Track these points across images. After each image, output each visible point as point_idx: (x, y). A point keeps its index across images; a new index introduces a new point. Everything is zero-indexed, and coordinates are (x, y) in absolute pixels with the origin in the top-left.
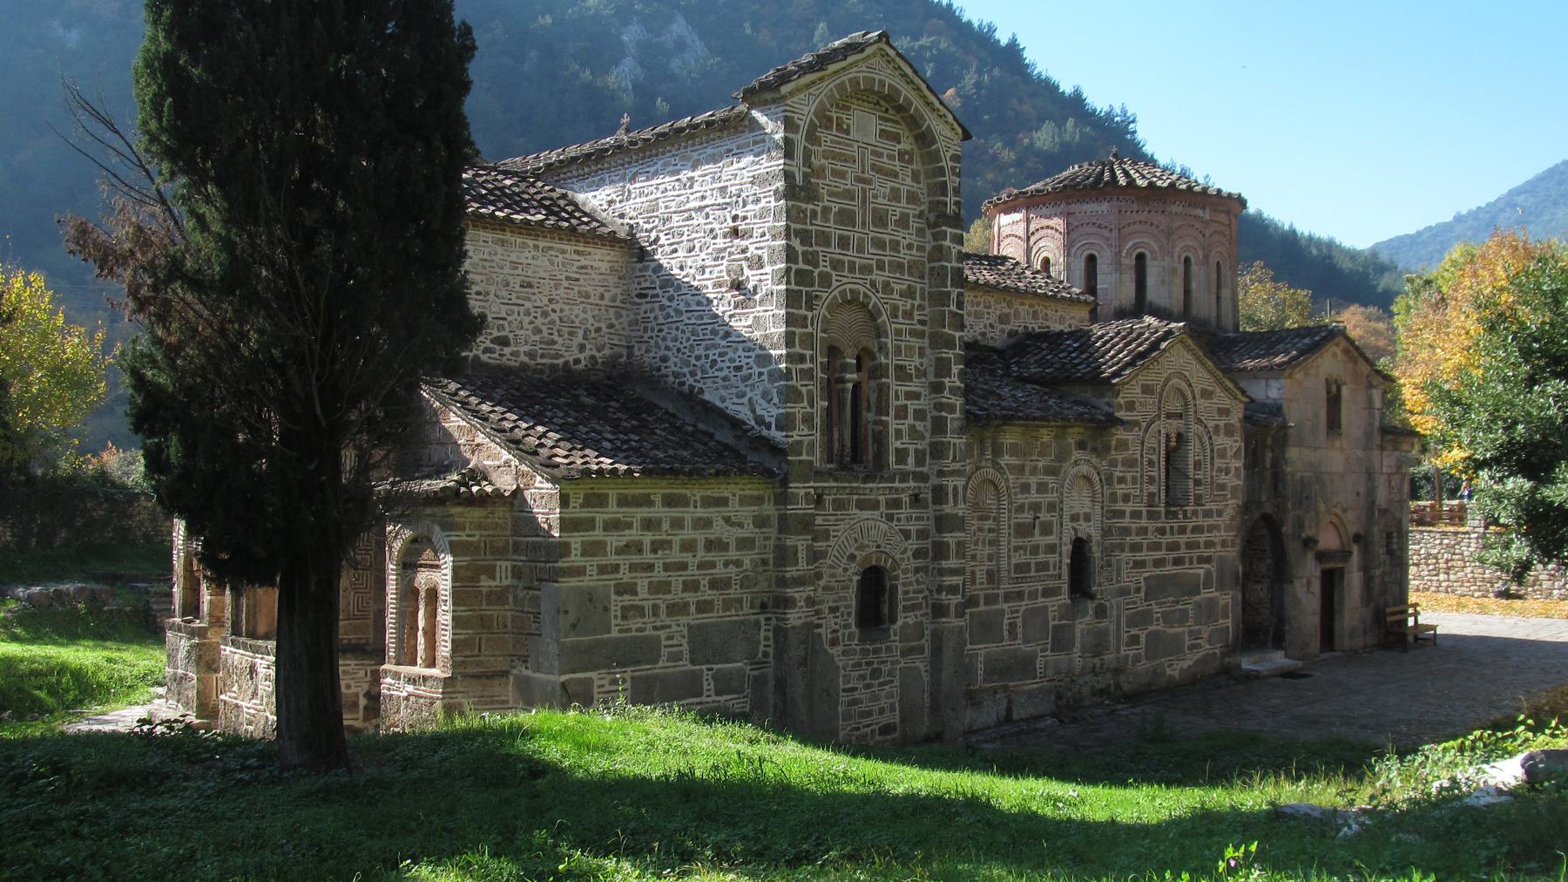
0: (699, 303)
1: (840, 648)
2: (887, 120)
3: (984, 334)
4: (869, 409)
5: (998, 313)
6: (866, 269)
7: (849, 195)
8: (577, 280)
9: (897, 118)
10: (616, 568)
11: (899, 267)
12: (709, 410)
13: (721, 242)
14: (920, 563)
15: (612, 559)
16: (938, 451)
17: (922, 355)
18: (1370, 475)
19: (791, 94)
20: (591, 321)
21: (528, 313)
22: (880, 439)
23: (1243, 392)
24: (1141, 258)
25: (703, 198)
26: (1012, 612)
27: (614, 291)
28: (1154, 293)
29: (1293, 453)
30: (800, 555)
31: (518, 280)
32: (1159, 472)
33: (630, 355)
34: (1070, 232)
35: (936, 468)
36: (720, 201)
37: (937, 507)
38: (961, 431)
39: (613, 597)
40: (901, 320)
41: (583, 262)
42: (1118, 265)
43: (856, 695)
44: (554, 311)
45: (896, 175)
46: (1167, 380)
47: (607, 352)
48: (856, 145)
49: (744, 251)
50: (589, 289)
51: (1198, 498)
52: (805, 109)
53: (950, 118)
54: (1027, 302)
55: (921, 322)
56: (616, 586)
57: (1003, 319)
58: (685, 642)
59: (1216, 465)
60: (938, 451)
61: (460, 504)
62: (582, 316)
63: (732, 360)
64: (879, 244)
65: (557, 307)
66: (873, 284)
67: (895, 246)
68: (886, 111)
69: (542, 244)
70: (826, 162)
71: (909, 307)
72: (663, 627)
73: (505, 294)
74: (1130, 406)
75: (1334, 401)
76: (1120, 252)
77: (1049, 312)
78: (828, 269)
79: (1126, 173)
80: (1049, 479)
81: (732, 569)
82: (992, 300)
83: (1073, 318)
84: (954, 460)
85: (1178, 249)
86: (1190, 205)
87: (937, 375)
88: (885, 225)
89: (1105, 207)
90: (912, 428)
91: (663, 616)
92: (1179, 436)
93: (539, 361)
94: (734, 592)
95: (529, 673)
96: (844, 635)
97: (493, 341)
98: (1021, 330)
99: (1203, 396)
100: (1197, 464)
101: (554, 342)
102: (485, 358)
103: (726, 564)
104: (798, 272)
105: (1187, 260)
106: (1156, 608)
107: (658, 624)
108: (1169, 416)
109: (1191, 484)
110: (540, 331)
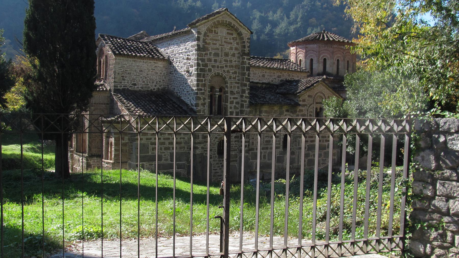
0: (181, 76)
1: (213, 159)
2: (229, 30)
3: (272, 81)
4: (223, 102)
5: (277, 75)
6: (222, 67)
7: (217, 49)
8: (154, 69)
9: (232, 29)
10: (151, 139)
12: (183, 102)
13: (185, 61)
14: (236, 139)
15: (149, 137)
19: (199, 25)
20: (158, 79)
21: (141, 78)
22: (226, 109)
23: (342, 97)
24: (325, 60)
25: (182, 50)
26: (264, 152)
27: (164, 72)
28: (328, 69)
30: (200, 137)
31: (139, 70)
33: (168, 87)
34: (306, 52)
36: (185, 51)
38: (248, 107)
39: (150, 145)
40: (232, 80)
41: (156, 65)
42: (318, 62)
43: (217, 171)
44: (148, 77)
45: (231, 43)
46: (317, 94)
47: (162, 87)
48: (220, 37)
49: (189, 63)
50: (158, 72)
52: (203, 29)
53: (247, 29)
54: (287, 72)
55: (238, 80)
56: (151, 143)
57: (279, 77)
58: (169, 156)
61: (116, 123)
62: (156, 78)
63: (187, 90)
64: (226, 61)
65: (149, 76)
66: (224, 71)
67: (231, 61)
68: (229, 28)
69: (145, 61)
70: (210, 41)
71: (235, 76)
72: (163, 153)
73: (135, 73)
74: (304, 101)
76: (319, 58)
77: (294, 75)
78: (211, 68)
79: (327, 37)
81: (182, 140)
82: (275, 72)
83: (301, 76)
86: (340, 45)
87: (242, 93)
88: (228, 56)
89: (315, 45)
90: (235, 106)
91: (163, 150)
93: (144, 89)
94: (183, 145)
95: (131, 162)
96: (213, 156)
97: (132, 84)
98: (284, 80)
101: (148, 85)
102: (130, 88)
103: (180, 138)
104: (200, 69)
105: (338, 60)
106: (311, 153)
107: (162, 152)
110: (144, 82)
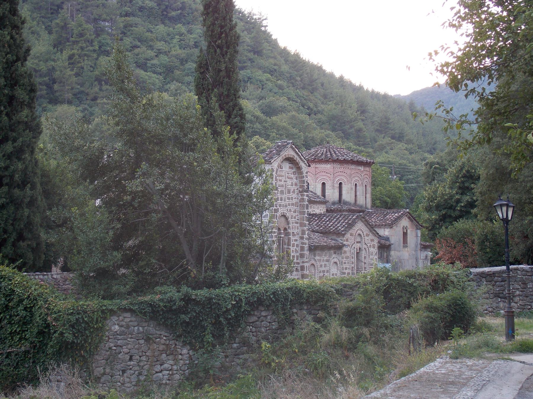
4: (285, 244)
6: (286, 206)
11: (293, 204)
16: (302, 256)
17: (298, 229)
18: (417, 259)
24: (341, 184)
29: (392, 253)
32: (354, 260)
35: (302, 261)
37: (302, 272)
51: (365, 268)
55: (298, 219)
59: (370, 258)
60: (302, 256)
75: (405, 234)
80: (327, 263)
84: (306, 258)
85: (353, 181)
88: (290, 193)
92: (360, 248)
99: (366, 236)
100: (365, 257)
105: (356, 184)
108: (357, 242)
109: (363, 263)
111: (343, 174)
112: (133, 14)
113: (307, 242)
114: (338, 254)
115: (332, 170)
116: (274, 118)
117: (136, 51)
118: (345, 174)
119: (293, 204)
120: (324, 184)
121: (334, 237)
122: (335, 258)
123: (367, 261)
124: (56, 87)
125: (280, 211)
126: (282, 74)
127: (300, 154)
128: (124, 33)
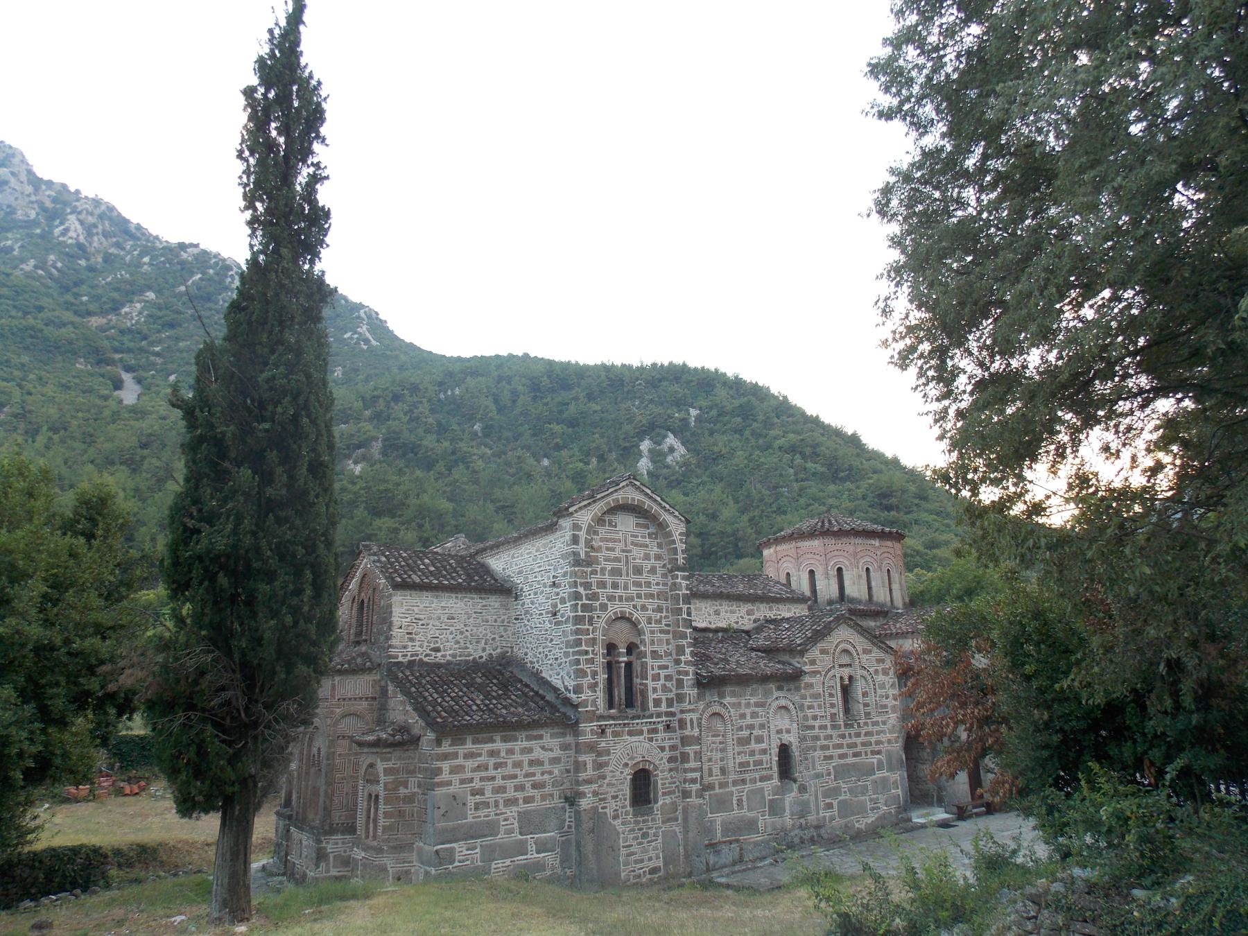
24: (840, 570)
51: (867, 715)
105: (868, 569)
109: (861, 707)
111: (841, 553)
112: (807, 479)
113: (691, 669)
114: (789, 690)
115: (822, 549)
116: (935, 551)
117: (810, 508)
118: (845, 554)
119: (651, 596)
120: (812, 572)
121: (786, 658)
122: (779, 698)
123: (870, 699)
124: (740, 544)
125: (610, 609)
126: (948, 515)
127: (659, 499)
128: (800, 495)
